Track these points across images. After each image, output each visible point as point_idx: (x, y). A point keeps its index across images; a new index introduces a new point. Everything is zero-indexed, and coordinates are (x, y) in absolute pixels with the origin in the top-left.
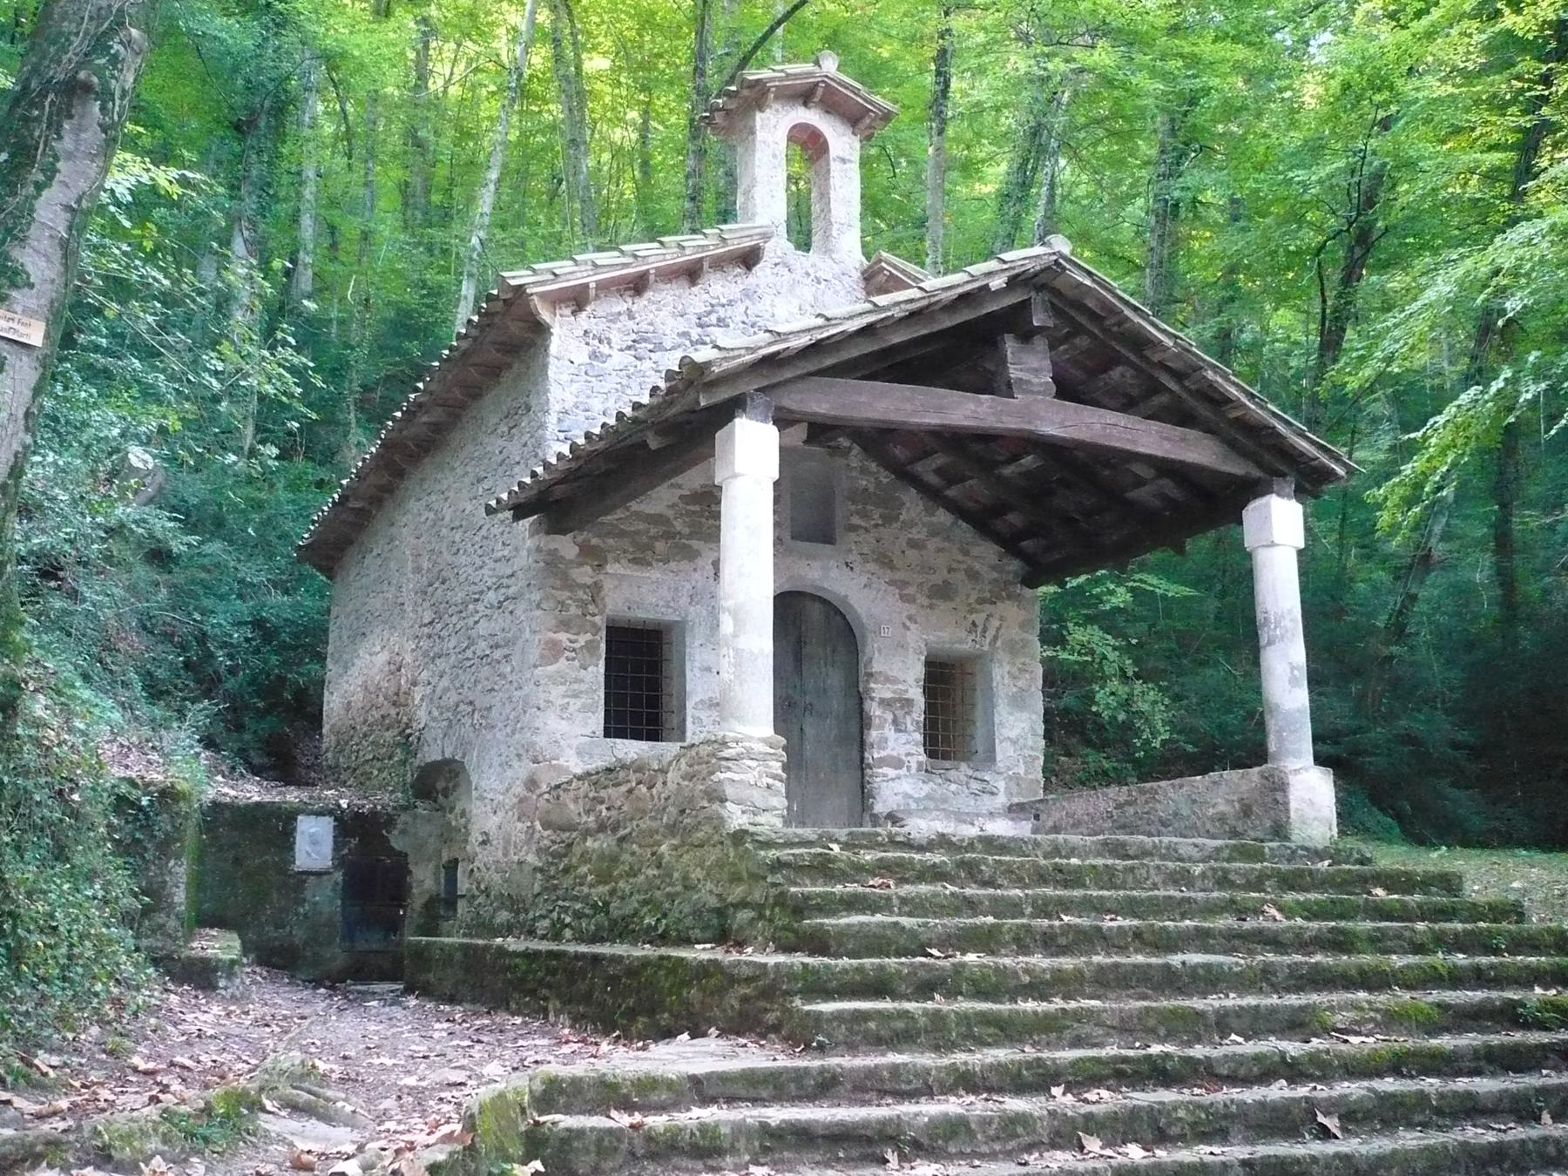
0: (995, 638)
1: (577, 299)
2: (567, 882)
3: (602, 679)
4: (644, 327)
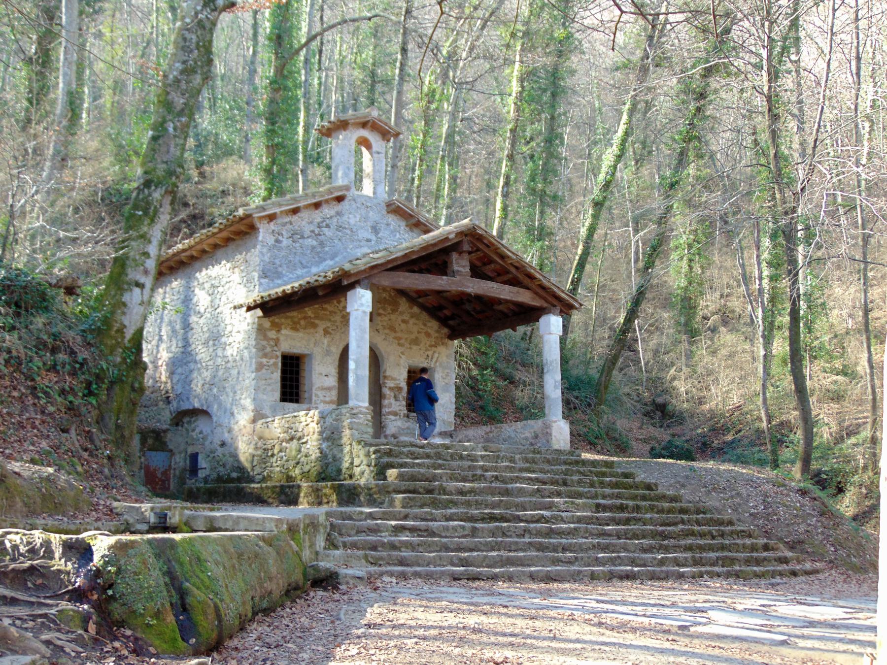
0: (436, 362)
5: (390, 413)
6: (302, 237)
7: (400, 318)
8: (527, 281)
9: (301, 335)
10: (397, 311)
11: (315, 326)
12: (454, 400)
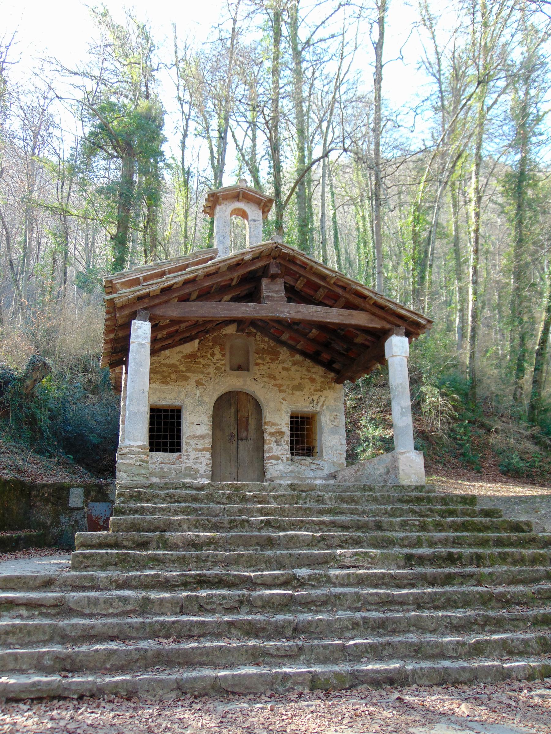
0: (323, 405)
5: (270, 458)
7: (280, 367)
8: (358, 301)
9: (171, 387)
10: (277, 359)
11: (186, 378)
12: (344, 442)
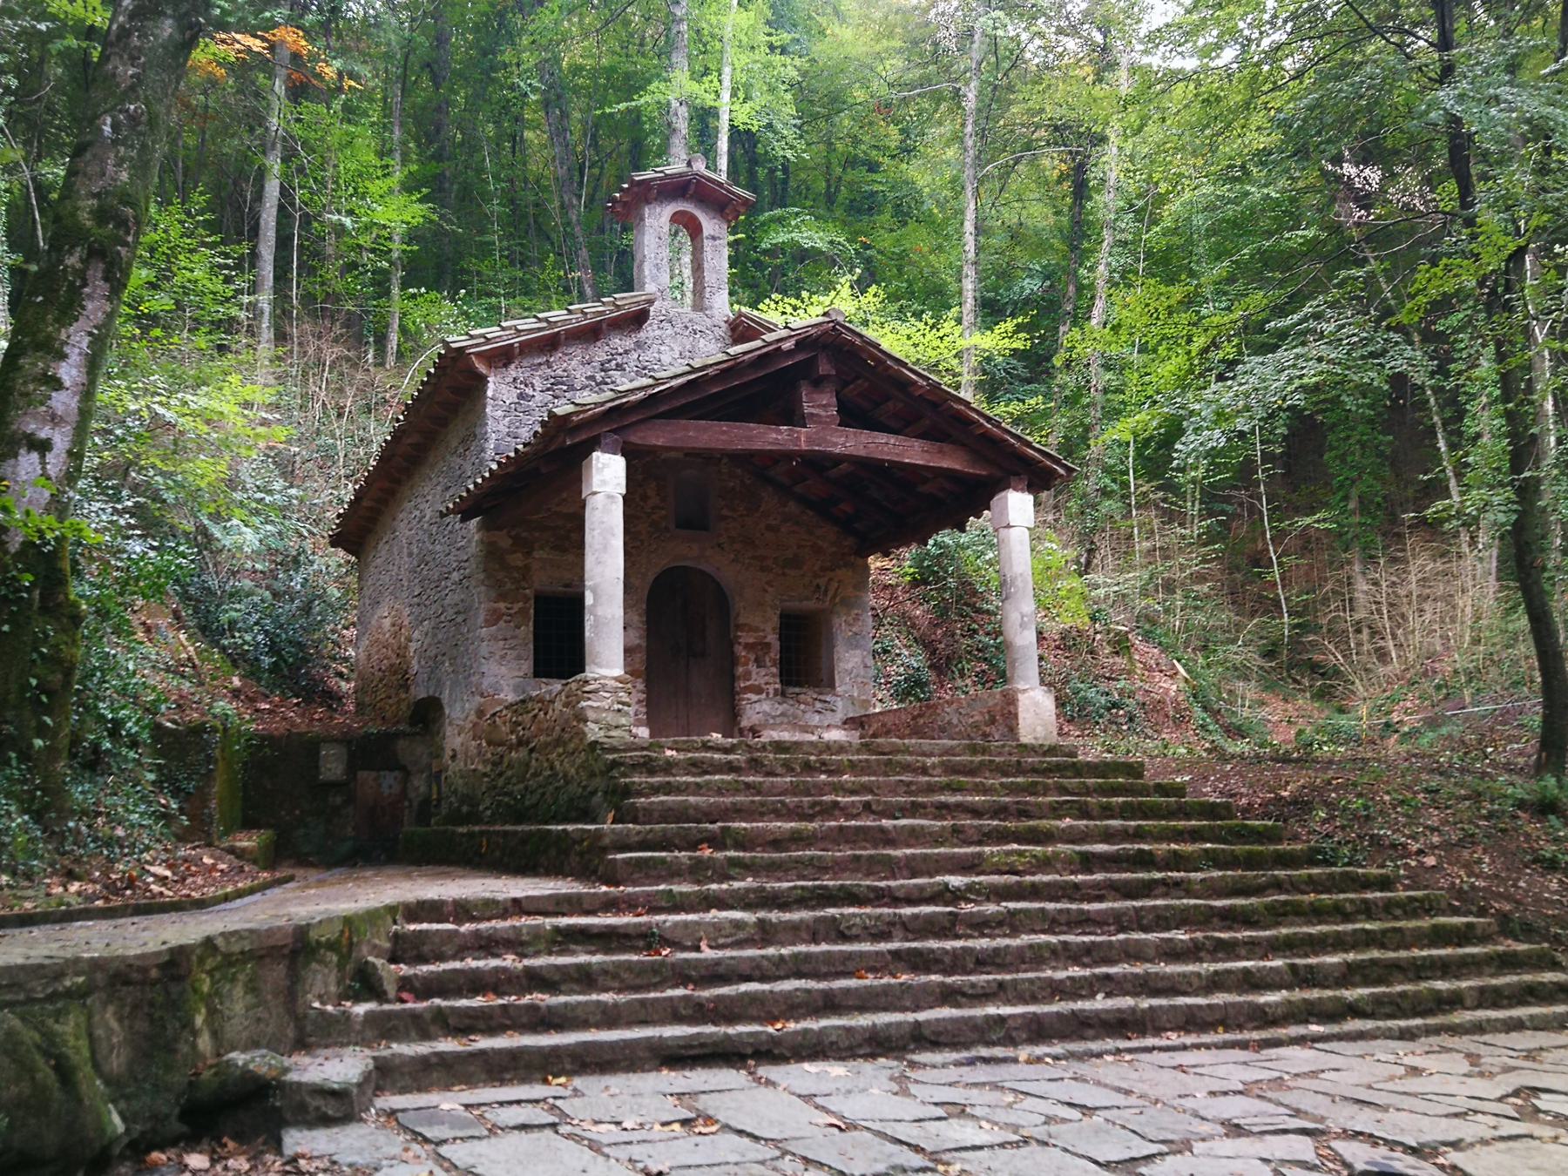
0: (834, 597)
1: (503, 357)
2: (501, 782)
3: (531, 636)
4: (559, 372)
6: (571, 388)
